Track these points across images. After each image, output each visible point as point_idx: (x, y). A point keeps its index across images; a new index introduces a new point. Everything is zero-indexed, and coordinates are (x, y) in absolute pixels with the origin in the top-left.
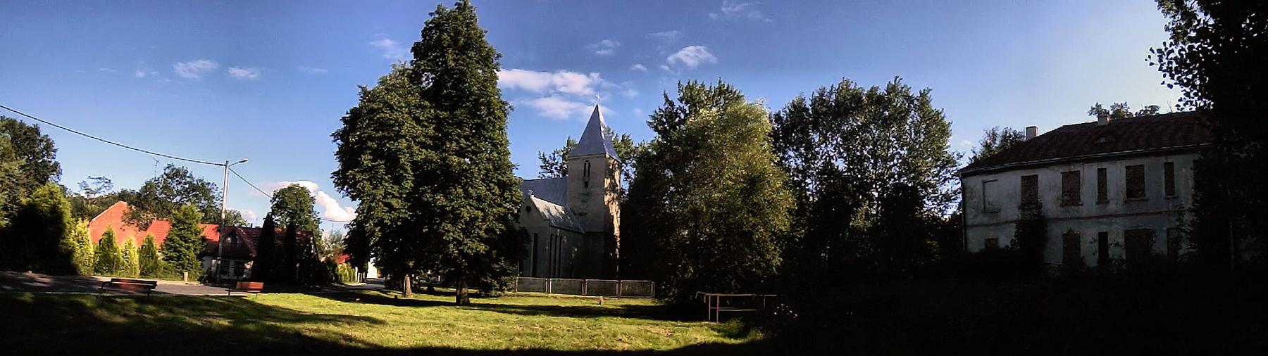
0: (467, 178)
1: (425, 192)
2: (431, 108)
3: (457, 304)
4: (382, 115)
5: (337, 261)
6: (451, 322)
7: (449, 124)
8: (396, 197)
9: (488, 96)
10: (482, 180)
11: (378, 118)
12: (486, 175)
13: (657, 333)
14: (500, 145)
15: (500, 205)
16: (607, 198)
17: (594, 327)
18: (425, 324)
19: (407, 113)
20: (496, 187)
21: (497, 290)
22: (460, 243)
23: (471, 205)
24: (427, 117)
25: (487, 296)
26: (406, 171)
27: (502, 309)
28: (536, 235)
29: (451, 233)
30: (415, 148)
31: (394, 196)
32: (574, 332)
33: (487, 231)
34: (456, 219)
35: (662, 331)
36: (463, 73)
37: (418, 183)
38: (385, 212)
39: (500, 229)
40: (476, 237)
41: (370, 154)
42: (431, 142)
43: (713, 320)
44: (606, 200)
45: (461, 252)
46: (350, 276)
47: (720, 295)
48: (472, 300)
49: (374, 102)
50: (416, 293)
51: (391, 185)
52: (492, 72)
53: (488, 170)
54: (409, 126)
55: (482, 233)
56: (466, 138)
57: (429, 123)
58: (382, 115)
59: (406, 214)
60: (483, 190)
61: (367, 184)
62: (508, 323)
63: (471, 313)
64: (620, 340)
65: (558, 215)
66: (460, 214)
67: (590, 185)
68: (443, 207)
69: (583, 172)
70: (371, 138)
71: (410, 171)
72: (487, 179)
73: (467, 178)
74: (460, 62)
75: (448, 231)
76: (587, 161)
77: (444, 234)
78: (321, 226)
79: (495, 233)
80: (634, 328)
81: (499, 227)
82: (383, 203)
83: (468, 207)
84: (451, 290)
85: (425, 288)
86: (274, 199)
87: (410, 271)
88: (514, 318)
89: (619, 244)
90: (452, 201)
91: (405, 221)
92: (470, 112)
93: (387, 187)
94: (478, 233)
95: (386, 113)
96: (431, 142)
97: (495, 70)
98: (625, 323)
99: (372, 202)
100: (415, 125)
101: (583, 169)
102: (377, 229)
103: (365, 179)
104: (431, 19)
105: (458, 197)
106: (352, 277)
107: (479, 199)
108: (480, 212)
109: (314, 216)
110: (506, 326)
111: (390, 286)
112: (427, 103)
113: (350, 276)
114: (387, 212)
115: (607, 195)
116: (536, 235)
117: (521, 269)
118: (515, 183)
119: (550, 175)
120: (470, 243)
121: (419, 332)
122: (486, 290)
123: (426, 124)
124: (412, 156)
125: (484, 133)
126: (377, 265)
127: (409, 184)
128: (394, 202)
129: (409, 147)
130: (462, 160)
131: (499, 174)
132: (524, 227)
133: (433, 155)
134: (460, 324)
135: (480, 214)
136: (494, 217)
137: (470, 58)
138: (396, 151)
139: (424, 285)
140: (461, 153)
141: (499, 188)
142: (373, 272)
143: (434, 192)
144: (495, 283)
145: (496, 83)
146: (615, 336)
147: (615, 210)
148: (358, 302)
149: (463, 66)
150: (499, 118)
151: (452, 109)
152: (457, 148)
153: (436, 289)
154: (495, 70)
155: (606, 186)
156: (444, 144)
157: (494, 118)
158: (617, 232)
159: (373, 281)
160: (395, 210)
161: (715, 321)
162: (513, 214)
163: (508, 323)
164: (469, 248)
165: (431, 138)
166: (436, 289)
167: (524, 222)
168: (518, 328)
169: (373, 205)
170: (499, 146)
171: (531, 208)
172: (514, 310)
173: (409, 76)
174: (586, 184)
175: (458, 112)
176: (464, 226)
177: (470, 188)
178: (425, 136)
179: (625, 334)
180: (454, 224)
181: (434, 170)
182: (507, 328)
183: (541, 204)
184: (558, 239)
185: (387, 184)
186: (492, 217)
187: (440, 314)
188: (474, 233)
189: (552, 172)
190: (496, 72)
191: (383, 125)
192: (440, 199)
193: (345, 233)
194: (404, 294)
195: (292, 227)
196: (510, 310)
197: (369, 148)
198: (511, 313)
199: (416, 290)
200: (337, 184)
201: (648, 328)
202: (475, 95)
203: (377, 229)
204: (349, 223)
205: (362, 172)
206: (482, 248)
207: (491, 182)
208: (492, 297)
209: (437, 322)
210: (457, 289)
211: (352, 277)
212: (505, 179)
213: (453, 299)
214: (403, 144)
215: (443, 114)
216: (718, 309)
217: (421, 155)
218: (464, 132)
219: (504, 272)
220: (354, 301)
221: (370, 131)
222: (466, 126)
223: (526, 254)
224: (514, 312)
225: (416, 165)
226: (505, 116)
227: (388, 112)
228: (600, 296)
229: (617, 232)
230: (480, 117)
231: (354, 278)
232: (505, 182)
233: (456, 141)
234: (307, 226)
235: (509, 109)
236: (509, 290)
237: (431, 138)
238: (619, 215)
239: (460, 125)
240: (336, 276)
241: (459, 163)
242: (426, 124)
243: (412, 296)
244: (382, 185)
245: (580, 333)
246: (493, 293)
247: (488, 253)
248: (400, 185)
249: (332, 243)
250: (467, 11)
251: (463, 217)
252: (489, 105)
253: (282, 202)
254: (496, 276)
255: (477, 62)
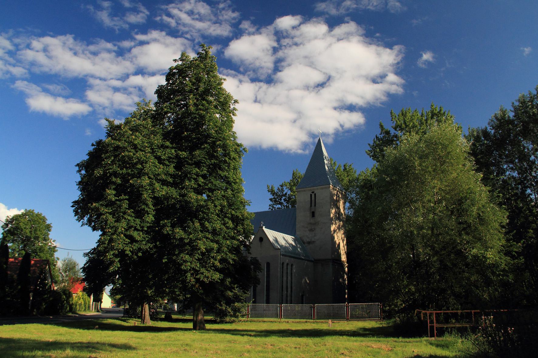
0: (203, 212)
1: (164, 226)
2: (172, 148)
3: (195, 328)
4: (127, 153)
5: (72, 290)
6: (189, 342)
7: (189, 164)
8: (138, 230)
9: (224, 138)
10: (218, 215)
11: (123, 156)
12: (221, 211)
13: (379, 348)
14: (234, 183)
15: (233, 238)
16: (333, 227)
17: (319, 345)
18: (165, 344)
19: (149, 152)
20: (230, 222)
21: (231, 316)
22: (196, 272)
23: (207, 238)
24: (169, 157)
25: (222, 322)
26: (147, 205)
27: (57, 322)
28: (268, 264)
29: (189, 263)
30: (157, 185)
31: (136, 229)
32: (301, 349)
33: (222, 261)
34: (194, 249)
35: (383, 346)
36: (202, 117)
37: (158, 217)
38: (126, 244)
39: (233, 259)
40: (212, 267)
41: (114, 189)
42: (170, 180)
43: (432, 336)
44: (332, 229)
45: (198, 280)
46: (85, 306)
47: (474, 311)
48: (208, 326)
49: (119, 140)
50: (154, 321)
51: (133, 218)
52: (228, 117)
53: (223, 207)
54: (152, 166)
55: (217, 263)
56: (204, 177)
57: (169, 162)
58: (127, 153)
59: (145, 246)
60: (218, 225)
61: (110, 217)
62: (240, 343)
63: (206, 336)
64: (343, 354)
65: (288, 245)
66: (197, 246)
67: (317, 214)
68: (182, 239)
69: (310, 202)
70: (115, 174)
71: (151, 207)
72: (222, 214)
73: (203, 212)
74: (200, 107)
75: (185, 261)
76: (313, 192)
77: (182, 264)
78: (56, 255)
79: (229, 263)
80: (357, 344)
81: (231, 258)
82: (125, 235)
83: (205, 240)
84: (187, 317)
85: (163, 316)
86: (7, 225)
87: (149, 299)
88: (246, 338)
89: (346, 269)
90: (190, 233)
91: (145, 252)
92: (208, 153)
93: (129, 220)
94: (213, 264)
95: (130, 152)
96: (170, 180)
97: (231, 115)
98: (348, 340)
99: (113, 234)
100: (157, 163)
101: (309, 199)
102: (117, 260)
103: (108, 213)
104: (174, 64)
105: (195, 230)
106: (87, 306)
107: (214, 232)
108: (215, 244)
109: (50, 244)
110: (237, 345)
111: (129, 314)
112: (168, 144)
113: (85, 306)
114: (129, 243)
115: (333, 224)
116: (268, 264)
117: (255, 296)
118: (247, 218)
119: (280, 206)
120: (206, 273)
121: (161, 352)
122: (221, 317)
123: (167, 163)
124: (153, 192)
125: (220, 172)
126: (113, 294)
127: (150, 218)
128: (135, 234)
129: (151, 184)
130: (199, 197)
131: (233, 209)
132: (255, 258)
133: (174, 192)
134: (197, 345)
135: (215, 246)
136: (228, 249)
137: (209, 102)
138: (139, 187)
139: (162, 313)
140: (199, 192)
141: (233, 222)
142: (107, 302)
143: (173, 226)
144: (229, 310)
145: (232, 127)
146: (337, 351)
147: (340, 238)
148: (97, 329)
149: (203, 110)
150: (234, 159)
151: (192, 149)
152: (196, 186)
153: (174, 317)
154: (231, 115)
155: (332, 215)
156: (183, 181)
157: (229, 159)
158: (344, 258)
159: (107, 311)
160: (137, 241)
161: (434, 336)
162: (245, 246)
163: (240, 343)
164: (205, 276)
165: (171, 176)
166: (174, 317)
167: (256, 253)
168: (248, 346)
169: (115, 237)
170: (233, 184)
171: (263, 238)
172: (246, 333)
173: (153, 117)
174: (313, 214)
175: (197, 152)
176: (200, 257)
177: (206, 222)
178: (165, 174)
179: (347, 349)
180: (191, 255)
181: (174, 205)
182: (238, 347)
183: (271, 234)
184: (289, 267)
185: (129, 218)
186: (226, 249)
187: (178, 337)
188: (209, 263)
189: (281, 204)
190: (232, 116)
191: (125, 163)
192: (179, 232)
193: (81, 262)
194: (143, 321)
195: (27, 257)
196: (242, 333)
197: (114, 183)
198: (243, 335)
199: (153, 317)
200: (76, 213)
201: (369, 344)
202: (213, 138)
203: (117, 260)
204: (88, 251)
205: (106, 206)
206: (217, 276)
207: (226, 217)
208: (226, 323)
209: (177, 342)
210: (194, 316)
211: (87, 306)
212: (238, 214)
213: (190, 325)
214: (145, 181)
215: (183, 154)
216: (435, 325)
217: (162, 191)
218: (202, 171)
219: (237, 299)
220: (93, 329)
221: (115, 168)
222: (204, 166)
223: (256, 281)
224: (239, 334)
225: (157, 201)
226: (240, 157)
227: (133, 150)
228: (328, 319)
229: (344, 258)
230: (216, 158)
231: (89, 307)
232: (237, 217)
233: (194, 179)
234: (42, 255)
235: (243, 151)
236: (243, 316)
237: (171, 176)
238: (345, 242)
239: (198, 164)
240: (71, 306)
241: (197, 201)
242: (167, 163)
243: (150, 323)
244: (125, 219)
245: (306, 349)
246: (228, 319)
247: (223, 281)
248: (141, 218)
249: (66, 272)
250: (209, 61)
251: (199, 249)
252: (224, 147)
253: (17, 228)
254: (229, 302)
255: (216, 107)
